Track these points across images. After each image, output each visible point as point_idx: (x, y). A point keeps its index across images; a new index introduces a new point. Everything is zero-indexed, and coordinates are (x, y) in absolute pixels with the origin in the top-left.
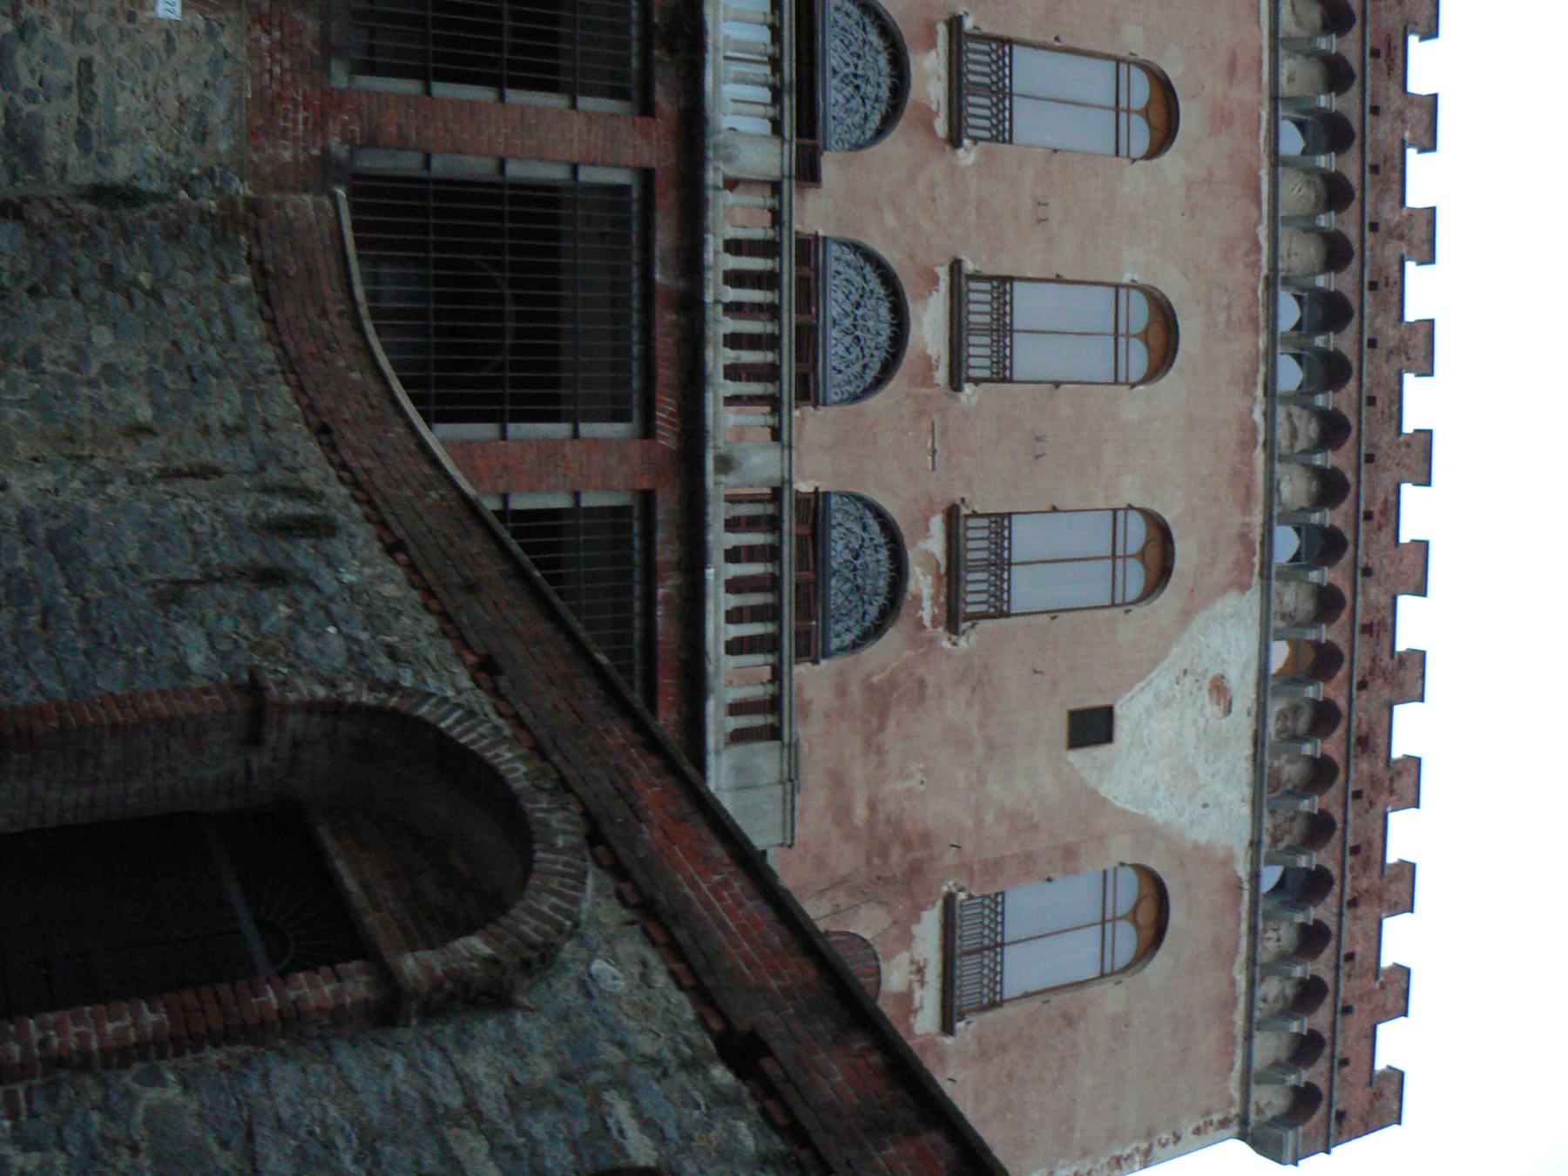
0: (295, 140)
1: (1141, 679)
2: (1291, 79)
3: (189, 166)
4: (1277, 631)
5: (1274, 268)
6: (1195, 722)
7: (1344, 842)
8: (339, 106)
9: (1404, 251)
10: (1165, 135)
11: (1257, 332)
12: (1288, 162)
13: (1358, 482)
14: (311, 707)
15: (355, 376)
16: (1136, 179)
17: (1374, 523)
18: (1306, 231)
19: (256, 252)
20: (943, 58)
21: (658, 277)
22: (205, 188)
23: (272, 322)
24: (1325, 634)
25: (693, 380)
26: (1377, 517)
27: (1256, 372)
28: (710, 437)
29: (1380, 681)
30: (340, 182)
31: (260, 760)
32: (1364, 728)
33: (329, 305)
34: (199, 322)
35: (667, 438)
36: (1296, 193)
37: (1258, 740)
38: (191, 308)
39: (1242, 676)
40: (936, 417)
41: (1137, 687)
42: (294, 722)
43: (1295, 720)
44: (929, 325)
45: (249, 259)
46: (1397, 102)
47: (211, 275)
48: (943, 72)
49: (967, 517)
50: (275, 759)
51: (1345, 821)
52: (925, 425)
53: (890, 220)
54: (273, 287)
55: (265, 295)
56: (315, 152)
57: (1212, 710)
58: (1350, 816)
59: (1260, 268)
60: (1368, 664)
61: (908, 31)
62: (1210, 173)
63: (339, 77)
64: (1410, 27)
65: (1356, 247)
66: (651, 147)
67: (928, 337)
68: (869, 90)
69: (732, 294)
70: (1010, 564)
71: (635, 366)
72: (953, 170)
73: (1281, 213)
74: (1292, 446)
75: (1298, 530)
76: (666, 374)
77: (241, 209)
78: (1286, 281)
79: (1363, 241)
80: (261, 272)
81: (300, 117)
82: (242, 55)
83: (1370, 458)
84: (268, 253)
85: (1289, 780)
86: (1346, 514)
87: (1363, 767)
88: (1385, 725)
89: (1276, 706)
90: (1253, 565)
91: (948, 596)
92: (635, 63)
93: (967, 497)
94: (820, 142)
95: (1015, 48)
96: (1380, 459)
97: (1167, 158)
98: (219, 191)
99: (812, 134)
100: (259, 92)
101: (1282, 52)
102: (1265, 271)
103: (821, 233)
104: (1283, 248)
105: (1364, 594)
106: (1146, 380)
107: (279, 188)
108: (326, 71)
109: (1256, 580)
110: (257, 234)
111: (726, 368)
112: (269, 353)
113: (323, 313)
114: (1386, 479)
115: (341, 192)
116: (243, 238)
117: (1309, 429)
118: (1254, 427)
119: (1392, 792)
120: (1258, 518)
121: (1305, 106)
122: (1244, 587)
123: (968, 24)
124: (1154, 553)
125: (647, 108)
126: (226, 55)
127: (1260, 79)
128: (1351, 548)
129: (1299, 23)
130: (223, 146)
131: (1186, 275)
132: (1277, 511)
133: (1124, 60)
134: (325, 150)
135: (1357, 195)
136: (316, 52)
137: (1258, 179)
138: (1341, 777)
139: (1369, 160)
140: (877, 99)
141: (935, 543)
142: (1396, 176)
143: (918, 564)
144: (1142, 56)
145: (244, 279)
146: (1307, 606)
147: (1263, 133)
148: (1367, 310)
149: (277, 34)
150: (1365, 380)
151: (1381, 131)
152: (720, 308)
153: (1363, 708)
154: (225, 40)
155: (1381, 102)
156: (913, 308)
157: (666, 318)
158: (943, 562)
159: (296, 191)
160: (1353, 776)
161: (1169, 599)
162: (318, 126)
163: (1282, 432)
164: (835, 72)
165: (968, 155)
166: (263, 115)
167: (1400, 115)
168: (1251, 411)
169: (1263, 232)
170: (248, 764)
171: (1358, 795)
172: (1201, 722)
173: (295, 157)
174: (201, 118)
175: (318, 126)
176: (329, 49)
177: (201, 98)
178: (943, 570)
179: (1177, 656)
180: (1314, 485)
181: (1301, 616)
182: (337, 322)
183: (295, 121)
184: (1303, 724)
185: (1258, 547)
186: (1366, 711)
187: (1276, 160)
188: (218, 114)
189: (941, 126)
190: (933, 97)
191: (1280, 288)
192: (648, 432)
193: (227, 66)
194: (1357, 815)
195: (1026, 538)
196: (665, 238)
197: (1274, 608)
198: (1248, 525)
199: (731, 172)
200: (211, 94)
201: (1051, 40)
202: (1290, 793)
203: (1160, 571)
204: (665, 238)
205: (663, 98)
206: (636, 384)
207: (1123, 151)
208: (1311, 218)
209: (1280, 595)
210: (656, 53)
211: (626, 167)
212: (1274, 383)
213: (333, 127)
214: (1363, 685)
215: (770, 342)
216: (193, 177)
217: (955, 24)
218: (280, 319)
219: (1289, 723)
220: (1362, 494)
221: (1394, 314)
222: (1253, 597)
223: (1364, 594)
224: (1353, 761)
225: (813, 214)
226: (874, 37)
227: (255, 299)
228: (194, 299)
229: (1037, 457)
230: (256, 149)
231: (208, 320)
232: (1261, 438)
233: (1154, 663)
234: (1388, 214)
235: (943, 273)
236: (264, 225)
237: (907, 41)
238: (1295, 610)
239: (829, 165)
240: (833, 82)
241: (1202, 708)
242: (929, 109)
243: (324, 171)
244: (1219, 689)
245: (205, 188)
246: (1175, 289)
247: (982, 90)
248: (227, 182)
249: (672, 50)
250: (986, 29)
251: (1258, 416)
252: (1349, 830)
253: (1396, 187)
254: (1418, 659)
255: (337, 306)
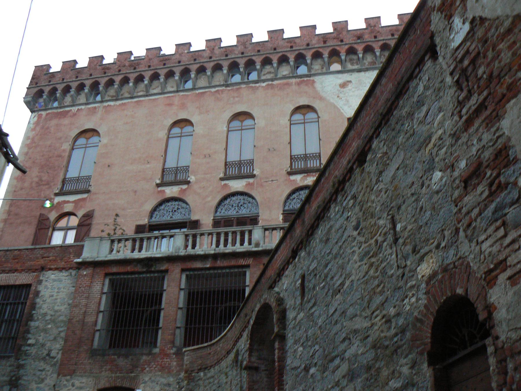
0: (171, 361)
1: (340, 110)
2: (172, 87)
3: (176, 388)
4: (326, 70)
5: (223, 85)
6: (353, 92)
7: (390, 39)
8: (164, 350)
9: (217, 47)
10: (187, 122)
11: (241, 88)
12: (194, 85)
13: (281, 52)
14: (250, 356)
15: (221, 345)
16: (199, 129)
17: (294, 45)
18: (213, 77)
19: (196, 371)
20: (167, 188)
21: (208, 266)
22: (182, 384)
23: (211, 366)
24: (326, 55)
25: (234, 255)
26: (291, 44)
27: (252, 87)
28: (248, 250)
29: (341, 35)
30: (182, 350)
31: (263, 367)
32: (354, 38)
33: (208, 352)
34: (210, 385)
35: (250, 261)
36: (202, 82)
37: (359, 71)
38: (207, 387)
39: (340, 78)
40: (262, 181)
41: (342, 111)
42: (253, 359)
43: (354, 59)
44: (237, 185)
45: (198, 373)
46: (178, 56)
47: (201, 382)
48: (170, 188)
49: (291, 169)
50: (263, 364)
51: (384, 40)
52: (265, 184)
53: (209, 199)
54: (204, 367)
55: (205, 368)
56: (174, 356)
57: (350, 86)
58: (382, 38)
59: (223, 89)
60: (335, 40)
61: (160, 198)
62: (197, 108)
63: (156, 350)
64: (158, 55)
65: (216, 62)
66: (176, 270)
67: (240, 185)
68: (176, 207)
69: (214, 246)
70: (305, 154)
71: (232, 271)
72: (196, 182)
73: (208, 85)
74: (273, 73)
75: (298, 67)
76: (233, 263)
77: (187, 375)
78: (226, 81)
79: (214, 61)
80: (200, 370)
81: (166, 360)
82: (150, 375)
83: (275, 49)
84: (196, 368)
85: (372, 59)
86: (291, 54)
87: (367, 37)
88: (354, 32)
89: (349, 66)
90: (307, 80)
91: (313, 172)
92: (156, 275)
93: (285, 170)
94: (188, 220)
95: (166, 167)
96: (275, 46)
97: (193, 121)
98: (182, 381)
99: (186, 223)
100: (160, 371)
101: (166, 91)
102: (224, 88)
103: (212, 218)
104: (218, 83)
105: (315, 45)
106: (254, 120)
107: (182, 365)
108: (155, 353)
109: (311, 78)
110: (192, 371)
111: (232, 246)
112: (216, 367)
113: (210, 353)
114: (281, 43)
115: (184, 350)
116: (193, 374)
117: (268, 68)
118: (268, 85)
119: (375, 26)
120: (294, 80)
121: (179, 82)
122: (314, 82)
123: (158, 182)
124: (303, 111)
125: (166, 271)
126: (150, 379)
127: (173, 96)
128: (301, 51)
129: (158, 87)
130: (172, 379)
131: (225, 111)
132: (291, 75)
133: (168, 136)
134: (174, 354)
135: (202, 64)
136: (150, 356)
137: (199, 93)
138: (370, 43)
139: (192, 62)
140: (178, 205)
141: (298, 178)
142: (197, 54)
143: (304, 182)
144: (166, 131)
145: (202, 374)
146: (319, 61)
147: (187, 93)
148: (233, 56)
149: (146, 366)
150: (252, 54)
151: (185, 60)
152: (217, 249)
153: (349, 40)
154: (147, 379)
155: (177, 61)
156: (233, 190)
157: (219, 263)
158: (303, 175)
159: (183, 361)
160: (369, 39)
161: (316, 105)
162: (168, 355)
163: (269, 76)
164: (171, 217)
165: (192, 178)
166: (165, 369)
167: (181, 55)
168: (263, 87)
169: (213, 90)
170: (263, 371)
171: (375, 37)
172: (353, 90)
173: (175, 361)
174: (165, 385)
175: (168, 355)
176: (150, 354)
177: (160, 385)
178: (306, 175)
179: (333, 100)
180: (284, 64)
181: (322, 63)
182: (212, 350)
183: (167, 361)
184: (355, 57)
185: (302, 79)
186: (350, 38)
187: (194, 89)
188: (163, 380)
189: (185, 187)
190: (177, 190)
191: (228, 83)
192: (248, 266)
193: (153, 378)
194: (382, 36)
195: (298, 150)
196: (198, 265)
197: (320, 72)
198: (295, 83)
199: (182, 248)
200: (159, 383)
201: (162, 158)
202: (376, 58)
203: (309, 108)
204: (198, 265)
205: (163, 268)
206: (236, 270)
207: (191, 134)
208: (208, 77)
209: (316, 70)
210: (153, 269)
211: (181, 275)
212: (256, 81)
213: (168, 352)
214: (342, 41)
215: (226, 234)
216: (179, 387)
217: (158, 185)
218: (210, 365)
219: (355, 62)
220: (285, 50)
221: (235, 48)
222: (316, 79)
223: (315, 45)
224: (364, 40)
225: (207, 221)
226: (162, 207)
227: (206, 371)
228: (205, 386)
229: (275, 150)
230: (173, 371)
231: (210, 383)
232: (270, 83)
233: (335, 107)
234: (206, 54)
235: (223, 183)
236: (190, 369)
237: (163, 198)
238: (320, 65)
239: (194, 218)
240: (174, 217)
241: (350, 90)
242: (180, 191)
243: (179, 354)
244: (343, 85)
245: (182, 384)
246: (228, 114)
247: (175, 176)
248: (180, 379)
249: (152, 266)
250: (160, 176)
251: (264, 84)
252: (386, 38)
253: (200, 53)
254: (335, 24)
255: (208, 350)
